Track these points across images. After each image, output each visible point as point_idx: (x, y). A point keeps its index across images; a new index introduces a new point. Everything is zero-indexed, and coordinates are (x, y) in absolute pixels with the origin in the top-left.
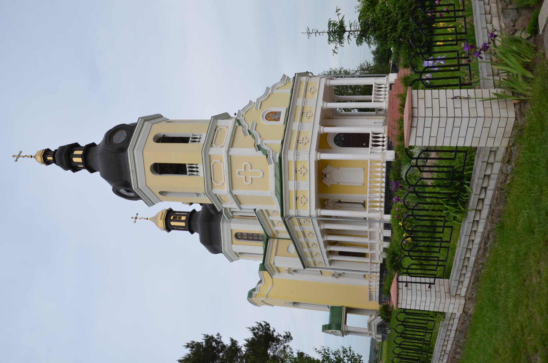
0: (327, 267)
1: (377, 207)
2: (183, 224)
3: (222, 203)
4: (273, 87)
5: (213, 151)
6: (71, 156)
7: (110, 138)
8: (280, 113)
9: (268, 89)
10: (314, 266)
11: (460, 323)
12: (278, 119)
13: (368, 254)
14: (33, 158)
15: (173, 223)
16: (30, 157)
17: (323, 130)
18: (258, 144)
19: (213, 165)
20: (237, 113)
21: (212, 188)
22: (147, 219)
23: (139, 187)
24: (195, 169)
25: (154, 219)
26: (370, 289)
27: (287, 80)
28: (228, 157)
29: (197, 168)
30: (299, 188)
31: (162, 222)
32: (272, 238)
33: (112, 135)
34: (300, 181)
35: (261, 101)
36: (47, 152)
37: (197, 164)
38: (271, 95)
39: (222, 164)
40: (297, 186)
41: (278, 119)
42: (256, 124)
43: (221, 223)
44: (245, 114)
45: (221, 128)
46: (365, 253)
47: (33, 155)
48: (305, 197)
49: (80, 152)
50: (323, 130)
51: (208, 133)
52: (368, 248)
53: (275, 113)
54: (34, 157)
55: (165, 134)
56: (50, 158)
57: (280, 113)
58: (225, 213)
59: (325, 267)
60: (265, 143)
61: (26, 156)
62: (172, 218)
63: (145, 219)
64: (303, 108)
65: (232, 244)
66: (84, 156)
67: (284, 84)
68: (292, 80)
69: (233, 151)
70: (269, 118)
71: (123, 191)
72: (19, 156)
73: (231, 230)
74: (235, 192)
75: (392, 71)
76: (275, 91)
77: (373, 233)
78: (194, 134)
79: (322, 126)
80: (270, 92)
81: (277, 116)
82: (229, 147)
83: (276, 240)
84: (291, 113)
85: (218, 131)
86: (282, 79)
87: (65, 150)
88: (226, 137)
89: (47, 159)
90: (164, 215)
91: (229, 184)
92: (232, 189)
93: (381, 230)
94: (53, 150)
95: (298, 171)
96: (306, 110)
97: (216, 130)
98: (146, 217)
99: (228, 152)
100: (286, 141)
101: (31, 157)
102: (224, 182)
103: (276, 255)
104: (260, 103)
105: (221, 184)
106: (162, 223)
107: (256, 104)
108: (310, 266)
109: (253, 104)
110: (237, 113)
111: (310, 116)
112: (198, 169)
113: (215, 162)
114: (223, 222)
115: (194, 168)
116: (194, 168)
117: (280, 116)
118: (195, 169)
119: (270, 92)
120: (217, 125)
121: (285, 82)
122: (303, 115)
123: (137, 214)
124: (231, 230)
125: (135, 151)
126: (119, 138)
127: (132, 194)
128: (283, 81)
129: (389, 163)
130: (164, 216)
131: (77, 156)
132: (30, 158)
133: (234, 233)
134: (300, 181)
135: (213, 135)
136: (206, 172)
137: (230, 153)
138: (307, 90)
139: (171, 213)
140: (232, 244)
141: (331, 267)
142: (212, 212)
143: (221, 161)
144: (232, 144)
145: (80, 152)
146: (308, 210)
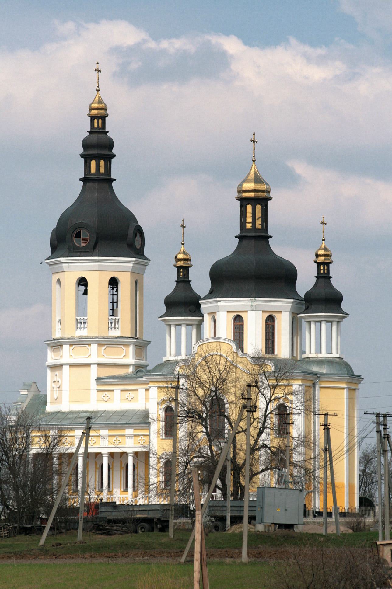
7: (72, 233)
11: (204, 517)
12: (327, 352)
13: (128, 494)
19: (86, 347)
30: (127, 438)
34: (133, 439)
40: (129, 436)
41: (327, 352)
46: (127, 491)
48: (120, 444)
65: (262, 311)
73: (281, 312)
75: (241, 539)
89: (92, 160)
95: (142, 437)
102: (74, 357)
103: (122, 390)
124: (281, 312)
133: (275, 315)
134: (133, 439)
140: (262, 311)
143: (125, 356)
146: (108, 445)
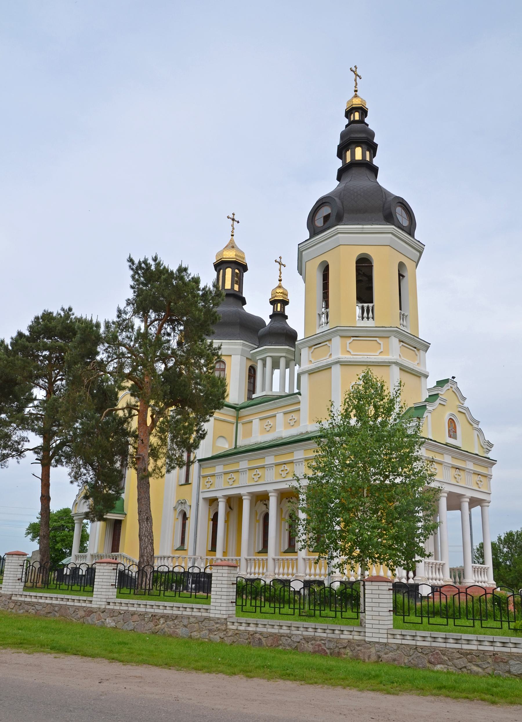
0: (200, 493)
1: (288, 569)
2: (228, 286)
3: (310, 347)
4: (480, 430)
5: (394, 341)
6: (364, 146)
8: (456, 438)
9: (478, 423)
10: (202, 474)
12: (450, 436)
14: (354, 93)
15: (229, 271)
16: (356, 89)
17: (444, 496)
18: (427, 407)
19: (376, 340)
20: (454, 380)
21: (341, 337)
22: (232, 235)
23: (339, 235)
24: (365, 314)
25: (232, 246)
26: (169, 557)
27: (487, 449)
28: (389, 362)
29: (368, 318)
31: (231, 256)
32: (238, 414)
33: (404, 206)
35: (466, 414)
36: (364, 112)
37: (373, 318)
38: (471, 427)
39: (378, 354)
42: (444, 405)
43: (242, 341)
44: (453, 391)
45: (417, 355)
46: (215, 551)
47: (357, 93)
49: (368, 159)
50: (444, 496)
51: (415, 338)
52: (223, 556)
53: (455, 432)
54: (356, 94)
55: (405, 278)
56: (357, 116)
57: (456, 438)
58: (266, 349)
59: (201, 491)
60: (428, 416)
61: (356, 84)
62: (237, 271)
63: (232, 232)
64: (463, 470)
66: (354, 164)
67: (483, 445)
68: (485, 455)
69: (395, 369)
70: (450, 423)
71: (326, 211)
72: (357, 75)
74: (336, 370)
76: (476, 433)
77: (253, 564)
78: (408, 317)
79: (448, 494)
80: (475, 426)
81: (452, 434)
82: (401, 365)
83: (233, 420)
84: (464, 455)
85: (414, 351)
86: (489, 442)
87: (370, 138)
88: (411, 362)
90: (240, 259)
91: (350, 362)
92: (341, 365)
93: (303, 576)
94: (366, 120)
96: (462, 473)
97: (415, 348)
98: (234, 234)
99: (396, 363)
100: (435, 445)
101: (356, 91)
104: (464, 412)
105: (348, 349)
106: (230, 255)
107: (462, 405)
108: (201, 469)
109: (462, 402)
110: (454, 380)
111: (457, 479)
112: (365, 319)
113: (380, 344)
114: (244, 345)
115: (368, 313)
116: (368, 313)
117: (452, 438)
118: (365, 314)
119: (475, 426)
120: (421, 351)
121: (484, 447)
122: (457, 470)
123: (238, 222)
125: (390, 235)
126: (400, 213)
127: (319, 222)
128: (487, 444)
129: (416, 587)
130: (240, 260)
131: (364, 155)
132: (354, 89)
135: (409, 343)
136: (367, 331)
137: (394, 365)
138: (480, 476)
139: (242, 271)
141: (201, 501)
142: (262, 330)
144: (404, 369)
145: (368, 159)
